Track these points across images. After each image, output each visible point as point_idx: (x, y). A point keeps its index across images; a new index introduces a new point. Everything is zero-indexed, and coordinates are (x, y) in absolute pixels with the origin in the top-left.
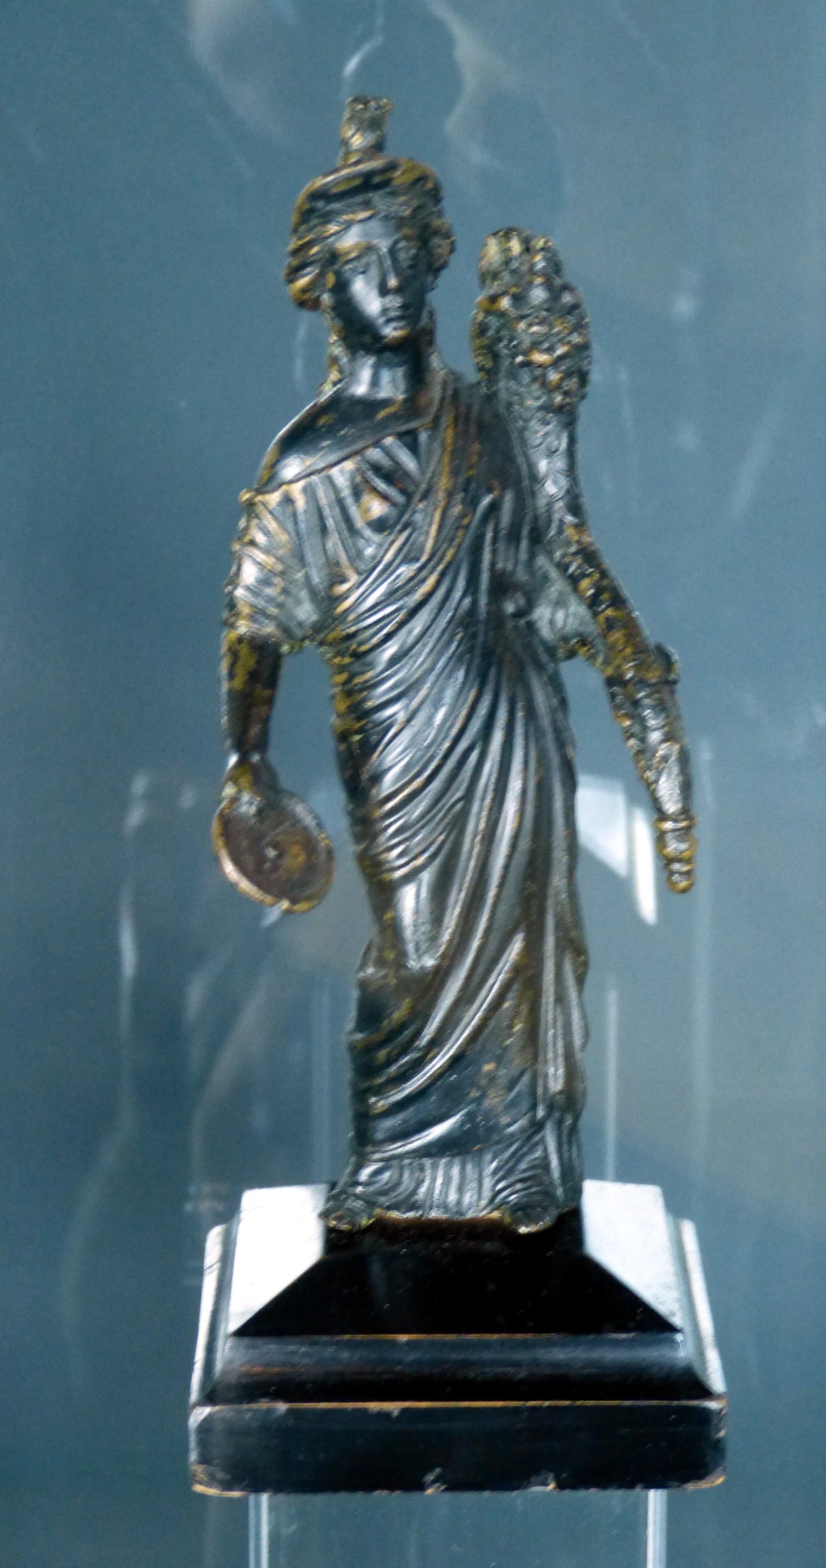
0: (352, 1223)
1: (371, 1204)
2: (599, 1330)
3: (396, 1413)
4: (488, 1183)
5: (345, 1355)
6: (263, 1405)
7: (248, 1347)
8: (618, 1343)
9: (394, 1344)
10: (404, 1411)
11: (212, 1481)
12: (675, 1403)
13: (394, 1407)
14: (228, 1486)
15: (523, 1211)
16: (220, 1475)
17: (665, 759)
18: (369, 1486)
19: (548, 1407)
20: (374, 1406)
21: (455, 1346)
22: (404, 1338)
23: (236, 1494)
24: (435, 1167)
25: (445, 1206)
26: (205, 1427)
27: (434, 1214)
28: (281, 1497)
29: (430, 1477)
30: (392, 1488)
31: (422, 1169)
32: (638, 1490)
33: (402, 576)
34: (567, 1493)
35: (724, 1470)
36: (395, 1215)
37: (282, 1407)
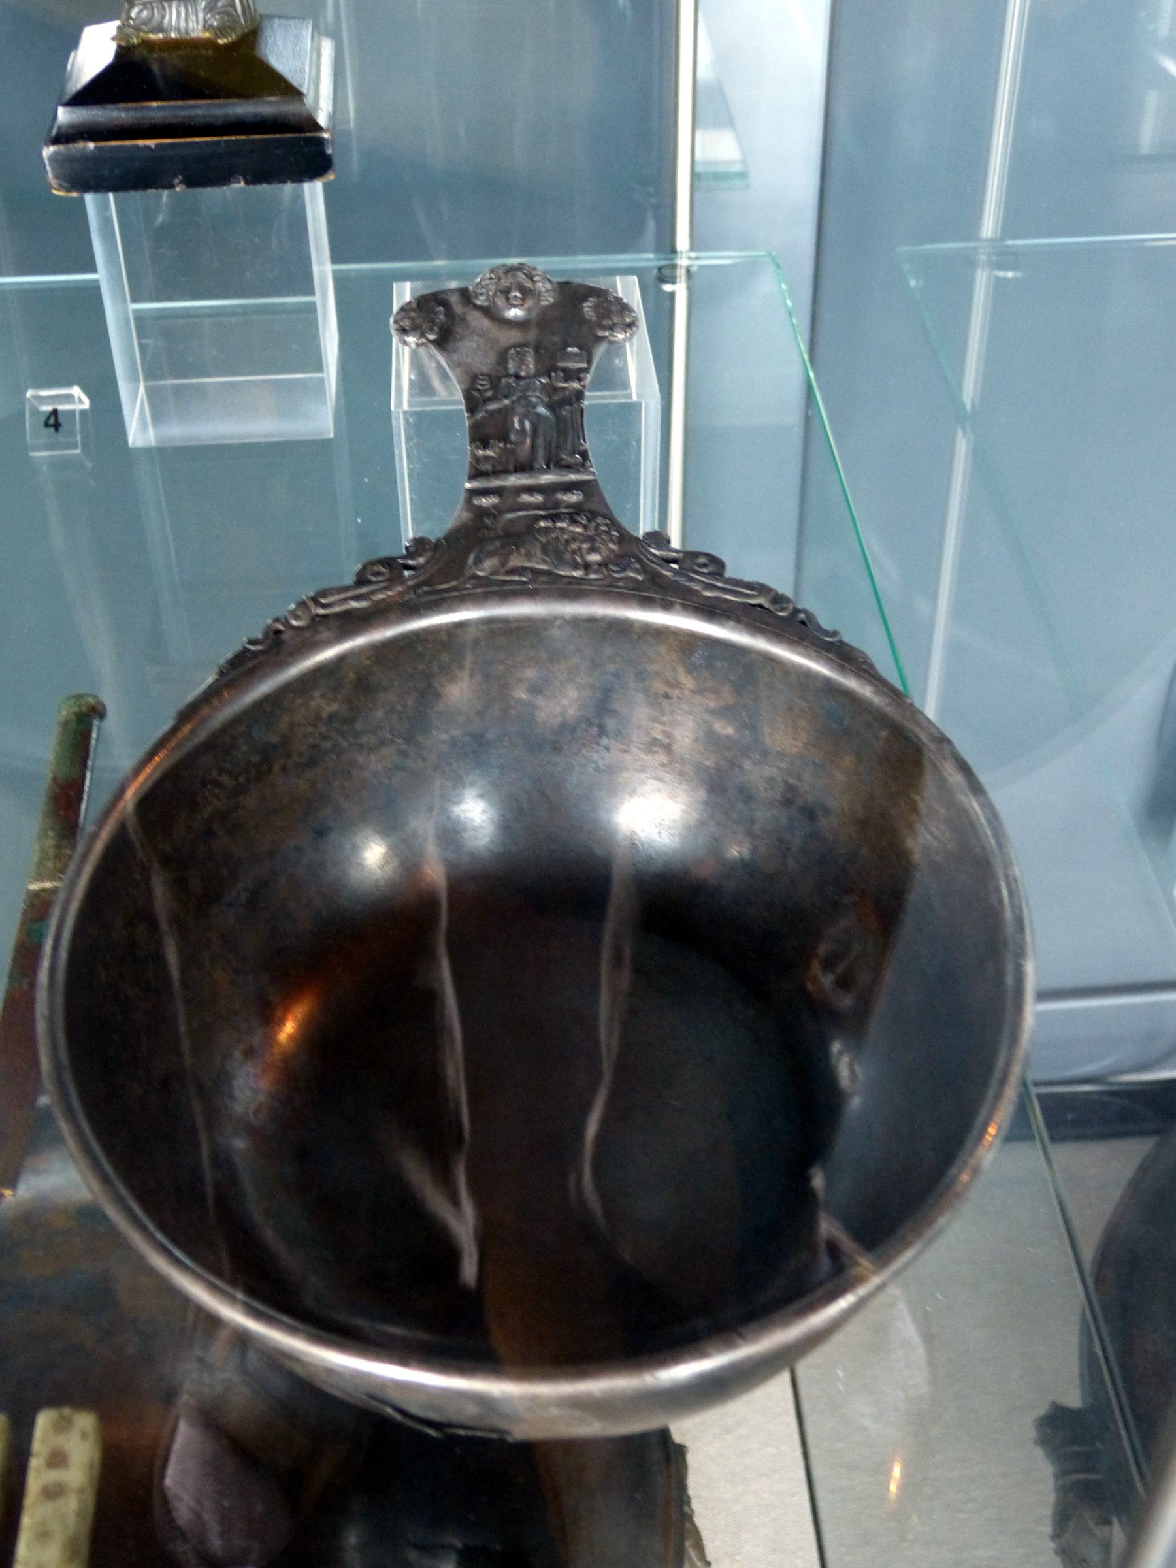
0: (128, 41)
1: (137, 29)
2: (260, 96)
3: (153, 146)
4: (201, 16)
5: (123, 115)
6: (81, 145)
7: (70, 112)
8: (270, 103)
9: (149, 108)
10: (157, 145)
11: (61, 188)
12: (303, 135)
13: (151, 143)
14: (68, 190)
15: (221, 31)
16: (64, 184)
17: (664, 732)
18: (145, 187)
19: (236, 140)
20: (141, 143)
21: (182, 108)
22: (154, 104)
23: (75, 194)
24: (170, 7)
25: (178, 29)
26: (53, 158)
27: (173, 35)
28: (122, 195)
29: (176, 181)
30: (268, 182)
31: (164, 8)
32: (160, 191)
33: (1065, 1195)
34: (251, 187)
35: (333, 171)
36: (152, 36)
37: (91, 145)
